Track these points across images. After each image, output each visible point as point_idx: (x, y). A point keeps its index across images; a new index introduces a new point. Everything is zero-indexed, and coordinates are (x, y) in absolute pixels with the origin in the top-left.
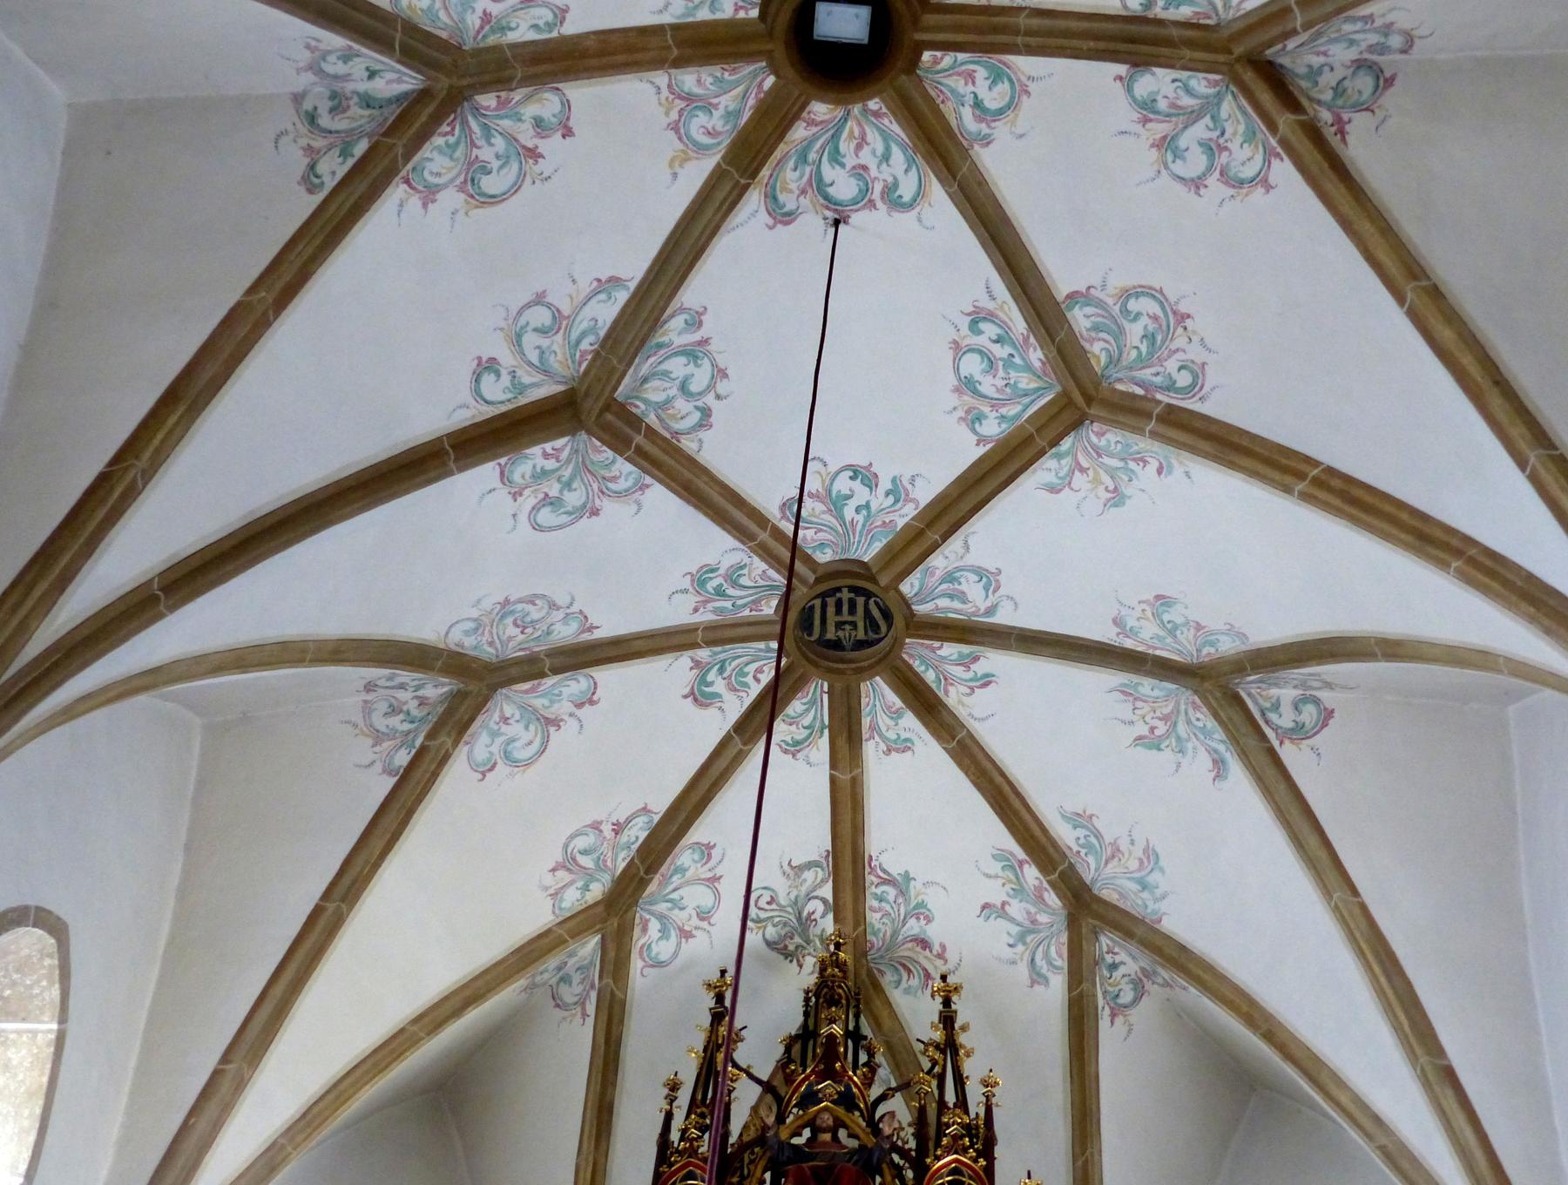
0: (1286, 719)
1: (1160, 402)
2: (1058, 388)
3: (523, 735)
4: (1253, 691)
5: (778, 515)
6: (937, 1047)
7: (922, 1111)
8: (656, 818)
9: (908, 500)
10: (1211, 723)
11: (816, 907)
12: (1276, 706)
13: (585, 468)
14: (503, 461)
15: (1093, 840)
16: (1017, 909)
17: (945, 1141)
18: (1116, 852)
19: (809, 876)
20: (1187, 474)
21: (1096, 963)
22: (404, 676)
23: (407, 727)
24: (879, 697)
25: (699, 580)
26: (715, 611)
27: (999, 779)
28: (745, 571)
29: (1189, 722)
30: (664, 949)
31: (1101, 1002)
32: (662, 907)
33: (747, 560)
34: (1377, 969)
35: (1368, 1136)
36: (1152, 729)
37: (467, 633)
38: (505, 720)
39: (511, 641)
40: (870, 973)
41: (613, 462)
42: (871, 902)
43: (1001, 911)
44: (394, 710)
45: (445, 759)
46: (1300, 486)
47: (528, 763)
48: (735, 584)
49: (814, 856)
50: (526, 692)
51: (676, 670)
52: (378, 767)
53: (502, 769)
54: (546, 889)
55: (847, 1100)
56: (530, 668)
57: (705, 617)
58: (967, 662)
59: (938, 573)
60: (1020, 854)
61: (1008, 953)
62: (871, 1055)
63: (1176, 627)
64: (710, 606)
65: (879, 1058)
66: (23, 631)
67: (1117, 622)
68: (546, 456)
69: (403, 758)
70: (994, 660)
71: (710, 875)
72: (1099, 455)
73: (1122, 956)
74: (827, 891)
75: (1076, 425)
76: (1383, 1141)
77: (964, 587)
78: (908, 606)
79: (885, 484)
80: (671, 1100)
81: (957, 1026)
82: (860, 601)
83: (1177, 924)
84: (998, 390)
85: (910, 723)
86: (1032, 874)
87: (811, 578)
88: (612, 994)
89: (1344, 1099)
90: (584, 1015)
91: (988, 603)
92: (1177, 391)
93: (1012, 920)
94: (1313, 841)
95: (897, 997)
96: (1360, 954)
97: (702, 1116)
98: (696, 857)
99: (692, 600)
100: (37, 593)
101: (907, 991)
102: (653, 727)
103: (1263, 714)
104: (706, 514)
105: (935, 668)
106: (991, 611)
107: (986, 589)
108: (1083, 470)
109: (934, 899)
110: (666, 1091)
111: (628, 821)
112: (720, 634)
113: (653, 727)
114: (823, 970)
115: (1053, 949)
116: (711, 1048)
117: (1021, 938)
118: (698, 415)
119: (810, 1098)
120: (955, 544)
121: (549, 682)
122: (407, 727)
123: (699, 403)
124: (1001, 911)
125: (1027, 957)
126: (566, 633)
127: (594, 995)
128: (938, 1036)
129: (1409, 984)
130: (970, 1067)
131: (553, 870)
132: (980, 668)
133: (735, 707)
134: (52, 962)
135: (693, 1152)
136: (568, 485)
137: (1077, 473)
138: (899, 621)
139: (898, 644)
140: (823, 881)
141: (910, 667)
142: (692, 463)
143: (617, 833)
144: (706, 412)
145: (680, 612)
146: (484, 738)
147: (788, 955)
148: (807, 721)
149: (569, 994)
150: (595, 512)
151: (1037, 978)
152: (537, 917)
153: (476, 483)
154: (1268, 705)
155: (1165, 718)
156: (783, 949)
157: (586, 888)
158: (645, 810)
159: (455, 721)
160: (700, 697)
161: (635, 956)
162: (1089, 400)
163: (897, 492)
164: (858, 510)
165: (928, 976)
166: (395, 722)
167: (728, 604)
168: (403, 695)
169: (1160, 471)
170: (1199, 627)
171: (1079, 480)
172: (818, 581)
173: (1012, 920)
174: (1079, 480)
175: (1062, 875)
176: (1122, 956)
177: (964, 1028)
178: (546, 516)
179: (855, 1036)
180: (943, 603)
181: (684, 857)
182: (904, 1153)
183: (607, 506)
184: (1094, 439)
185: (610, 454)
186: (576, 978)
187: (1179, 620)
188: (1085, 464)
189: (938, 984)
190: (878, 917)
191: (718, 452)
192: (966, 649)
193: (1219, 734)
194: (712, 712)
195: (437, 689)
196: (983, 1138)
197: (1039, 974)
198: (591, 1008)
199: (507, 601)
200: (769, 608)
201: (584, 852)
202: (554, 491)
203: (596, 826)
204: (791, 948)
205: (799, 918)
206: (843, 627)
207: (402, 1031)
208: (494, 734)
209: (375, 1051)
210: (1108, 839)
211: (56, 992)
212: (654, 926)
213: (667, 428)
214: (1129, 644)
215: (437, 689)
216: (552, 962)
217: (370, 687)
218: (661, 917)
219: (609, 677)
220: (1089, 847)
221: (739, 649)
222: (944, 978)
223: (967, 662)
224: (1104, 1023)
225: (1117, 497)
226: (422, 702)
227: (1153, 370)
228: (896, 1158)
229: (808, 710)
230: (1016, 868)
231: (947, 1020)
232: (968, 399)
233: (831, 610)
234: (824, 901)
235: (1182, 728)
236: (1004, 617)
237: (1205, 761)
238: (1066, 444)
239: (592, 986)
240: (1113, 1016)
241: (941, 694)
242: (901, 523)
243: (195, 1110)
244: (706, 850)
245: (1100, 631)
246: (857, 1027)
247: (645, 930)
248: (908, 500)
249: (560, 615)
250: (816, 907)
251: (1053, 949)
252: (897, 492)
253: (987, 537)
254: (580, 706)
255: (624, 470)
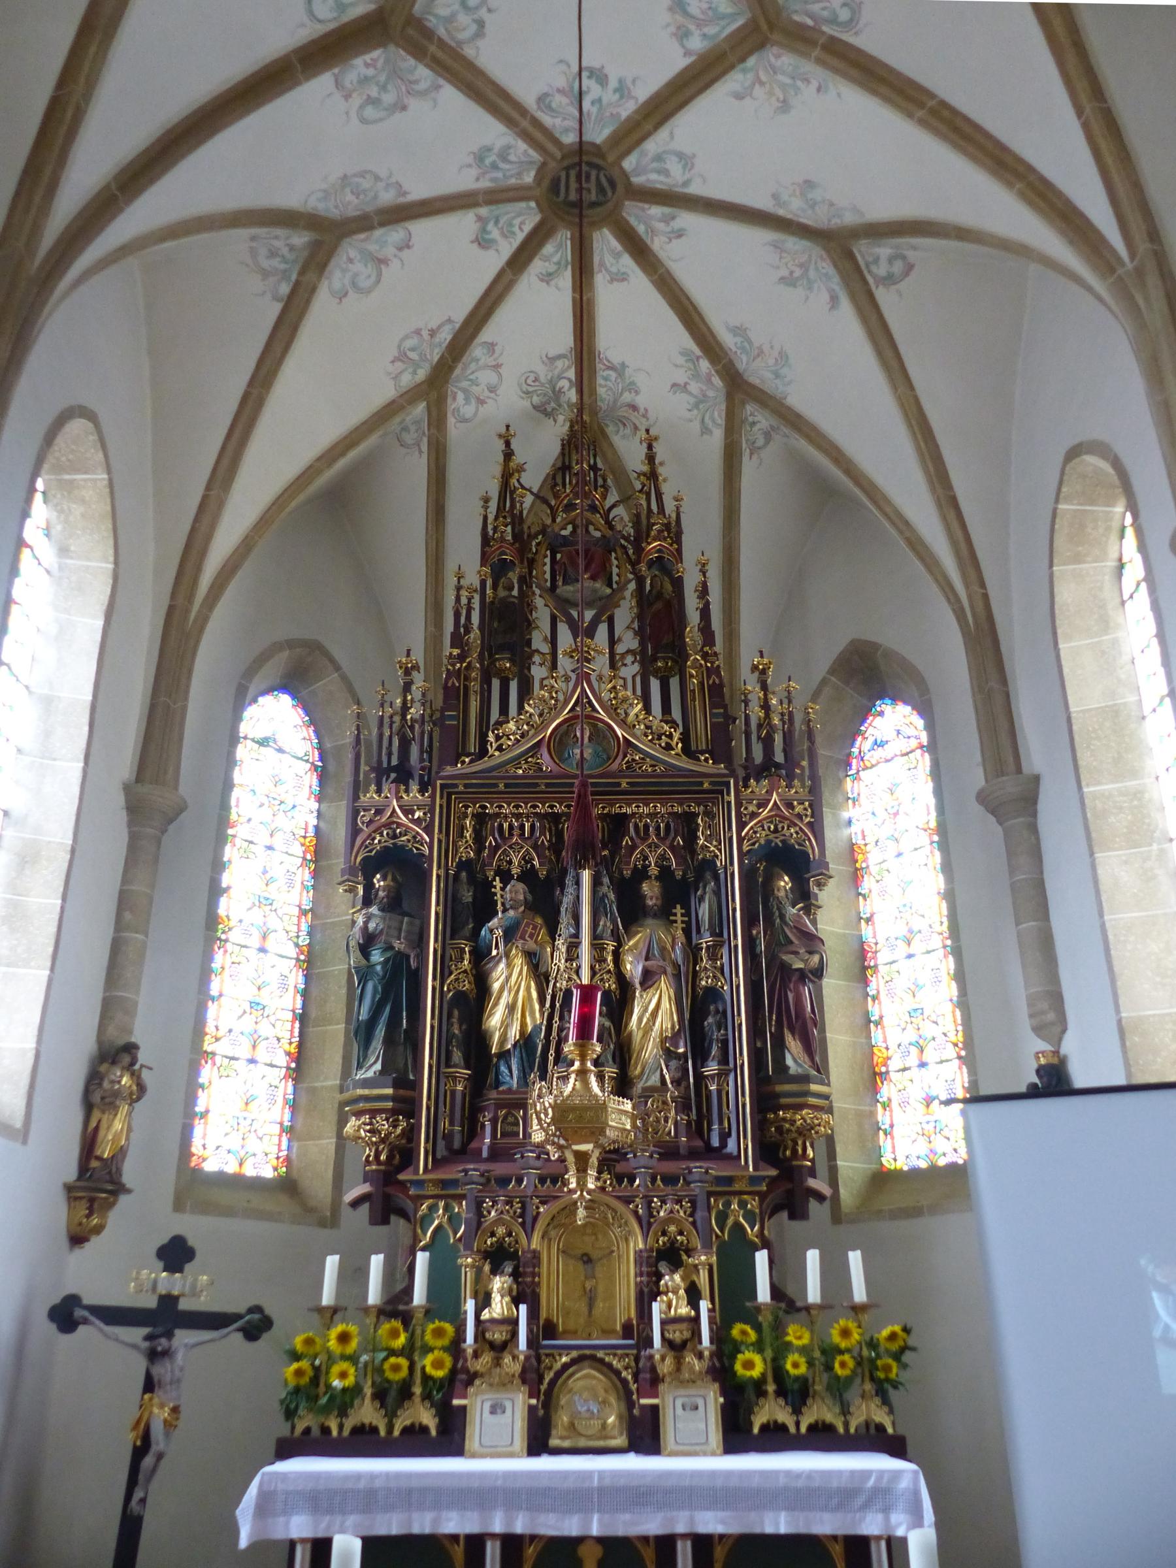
0: (882, 270)
1: (823, 33)
2: (749, 15)
3: (364, 271)
4: (863, 250)
5: (535, 107)
6: (644, 474)
7: (638, 516)
8: (458, 326)
9: (630, 97)
10: (831, 271)
11: (564, 384)
12: (877, 260)
13: (395, 73)
14: (336, 71)
15: (746, 344)
16: (694, 387)
17: (653, 533)
18: (761, 352)
19: (560, 364)
20: (839, 95)
21: (743, 422)
22: (279, 232)
23: (283, 266)
24: (605, 242)
25: (480, 157)
26: (492, 180)
27: (686, 302)
28: (512, 151)
29: (817, 269)
30: (468, 410)
31: (744, 446)
32: (465, 384)
33: (513, 142)
34: (919, 436)
35: (901, 532)
36: (792, 273)
37: (319, 200)
38: (351, 261)
39: (349, 204)
40: (599, 425)
41: (415, 68)
42: (600, 381)
43: (684, 388)
44: (273, 254)
45: (313, 290)
46: (920, 113)
47: (368, 291)
48: (505, 159)
49: (562, 351)
50: (362, 241)
51: (465, 223)
52: (269, 296)
53: (352, 295)
54: (390, 374)
55: (593, 508)
56: (364, 223)
57: (485, 184)
58: (667, 219)
59: (650, 155)
60: (698, 352)
61: (688, 415)
62: (605, 480)
63: (815, 203)
64: (488, 176)
65: (609, 481)
66: (36, 230)
67: (775, 196)
68: (367, 65)
69: (285, 289)
70: (687, 219)
71: (494, 363)
72: (775, 73)
73: (759, 418)
74: (571, 374)
75: (761, 46)
76: (908, 534)
77: (668, 166)
78: (628, 179)
79: (613, 83)
80: (486, 508)
81: (657, 462)
82: (594, 173)
83: (796, 400)
84: (703, 12)
85: (627, 262)
86: (705, 365)
87: (559, 155)
88: (438, 441)
89: (888, 510)
90: (421, 452)
91: (686, 178)
92: (839, 24)
93: (690, 394)
94: (889, 353)
95: (616, 440)
96: (910, 426)
97: (505, 517)
98: (485, 351)
99: (474, 172)
100: (37, 199)
101: (624, 437)
102: (447, 264)
103: (867, 266)
104: (484, 107)
105: (645, 223)
106: (686, 183)
107: (684, 167)
108: (762, 83)
109: (640, 380)
110: (482, 503)
111: (439, 327)
112: (496, 196)
113: (447, 264)
114: (572, 426)
115: (716, 413)
116: (506, 476)
117: (696, 406)
118: (474, 27)
119: (570, 507)
120: (663, 134)
121: (378, 233)
122: (283, 266)
123: (475, 17)
124: (684, 388)
125: (699, 418)
126: (387, 198)
127: (425, 440)
128: (646, 468)
129: (937, 446)
130: (665, 488)
131: (393, 362)
132: (677, 224)
133: (507, 249)
134: (94, 438)
135: (502, 539)
136: (384, 88)
137: (757, 86)
138: (620, 188)
139: (618, 206)
140: (569, 367)
141: (627, 222)
142: (470, 66)
143: (432, 336)
144: (481, 24)
145: (467, 181)
146: (337, 274)
147: (547, 414)
148: (556, 259)
149: (409, 438)
150: (404, 108)
151: (705, 430)
152: (386, 392)
153: (317, 90)
154: (871, 259)
155: (801, 266)
156: (544, 411)
157: (415, 373)
158: (449, 321)
159: (316, 263)
160: (482, 242)
161: (449, 415)
162: (772, 26)
163: (622, 90)
164: (593, 103)
165: (636, 428)
166: (276, 263)
167: (500, 175)
168: (277, 243)
169: (819, 90)
170: (832, 204)
171: (758, 91)
172: (563, 158)
173: (690, 394)
174: (758, 91)
175: (724, 366)
176: (759, 418)
177: (661, 464)
178: (369, 112)
179: (594, 468)
180: (654, 177)
181: (477, 351)
182: (626, 539)
183: (413, 103)
184: (772, 59)
185: (412, 61)
186: (413, 428)
187: (819, 199)
188: (763, 78)
189: (644, 435)
190: (605, 387)
191: (491, 57)
192: (667, 210)
193: (836, 279)
194: (491, 252)
195: (301, 239)
196: (674, 531)
197: (707, 429)
198: (425, 448)
199: (345, 176)
200: (529, 178)
201: (412, 349)
202: (374, 92)
203: (418, 332)
204: (549, 410)
205: (554, 391)
206: (583, 192)
207: (310, 467)
208: (344, 271)
209: (297, 479)
210: (756, 345)
211: (101, 455)
212: (460, 396)
213: (453, 39)
214: (781, 212)
215: (301, 239)
216: (397, 419)
217: (253, 238)
218: (465, 391)
219: (421, 229)
220: (743, 348)
221: (509, 207)
222: (647, 431)
223: (667, 219)
224: (746, 458)
225: (785, 106)
226: (292, 248)
227: (821, 5)
228: (623, 542)
229: (557, 252)
230: (694, 361)
231: (651, 458)
232: (679, 18)
233: (573, 179)
234: (570, 380)
235: (812, 273)
236: (696, 189)
237: (825, 297)
238: (751, 61)
239: (424, 433)
240: (751, 454)
241: (649, 242)
242: (624, 114)
243: (197, 519)
244: (491, 347)
245: (761, 201)
246: (595, 463)
247: (454, 399)
248: (630, 97)
249: (381, 185)
250: (564, 384)
251: (716, 413)
252: (622, 90)
253: (688, 129)
254: (400, 249)
255: (423, 74)
